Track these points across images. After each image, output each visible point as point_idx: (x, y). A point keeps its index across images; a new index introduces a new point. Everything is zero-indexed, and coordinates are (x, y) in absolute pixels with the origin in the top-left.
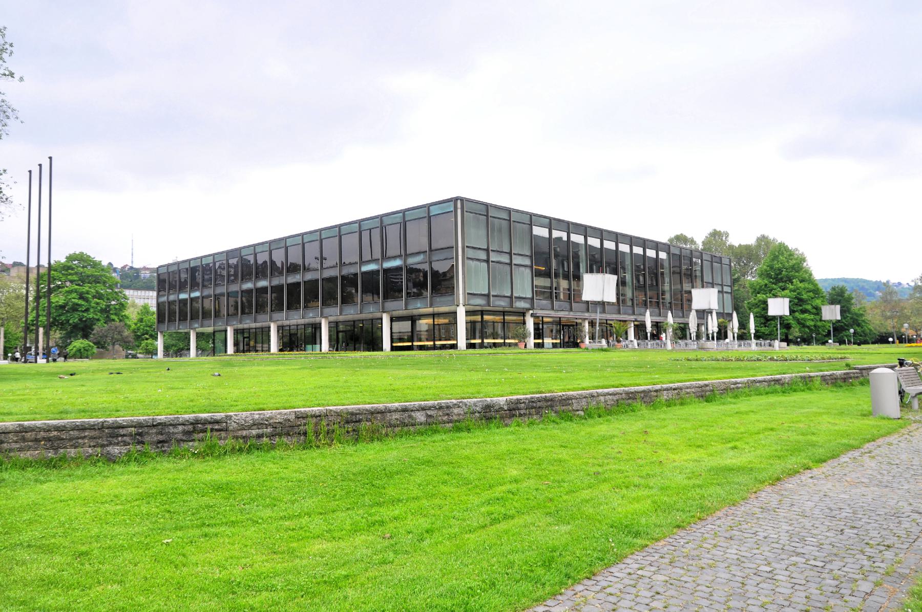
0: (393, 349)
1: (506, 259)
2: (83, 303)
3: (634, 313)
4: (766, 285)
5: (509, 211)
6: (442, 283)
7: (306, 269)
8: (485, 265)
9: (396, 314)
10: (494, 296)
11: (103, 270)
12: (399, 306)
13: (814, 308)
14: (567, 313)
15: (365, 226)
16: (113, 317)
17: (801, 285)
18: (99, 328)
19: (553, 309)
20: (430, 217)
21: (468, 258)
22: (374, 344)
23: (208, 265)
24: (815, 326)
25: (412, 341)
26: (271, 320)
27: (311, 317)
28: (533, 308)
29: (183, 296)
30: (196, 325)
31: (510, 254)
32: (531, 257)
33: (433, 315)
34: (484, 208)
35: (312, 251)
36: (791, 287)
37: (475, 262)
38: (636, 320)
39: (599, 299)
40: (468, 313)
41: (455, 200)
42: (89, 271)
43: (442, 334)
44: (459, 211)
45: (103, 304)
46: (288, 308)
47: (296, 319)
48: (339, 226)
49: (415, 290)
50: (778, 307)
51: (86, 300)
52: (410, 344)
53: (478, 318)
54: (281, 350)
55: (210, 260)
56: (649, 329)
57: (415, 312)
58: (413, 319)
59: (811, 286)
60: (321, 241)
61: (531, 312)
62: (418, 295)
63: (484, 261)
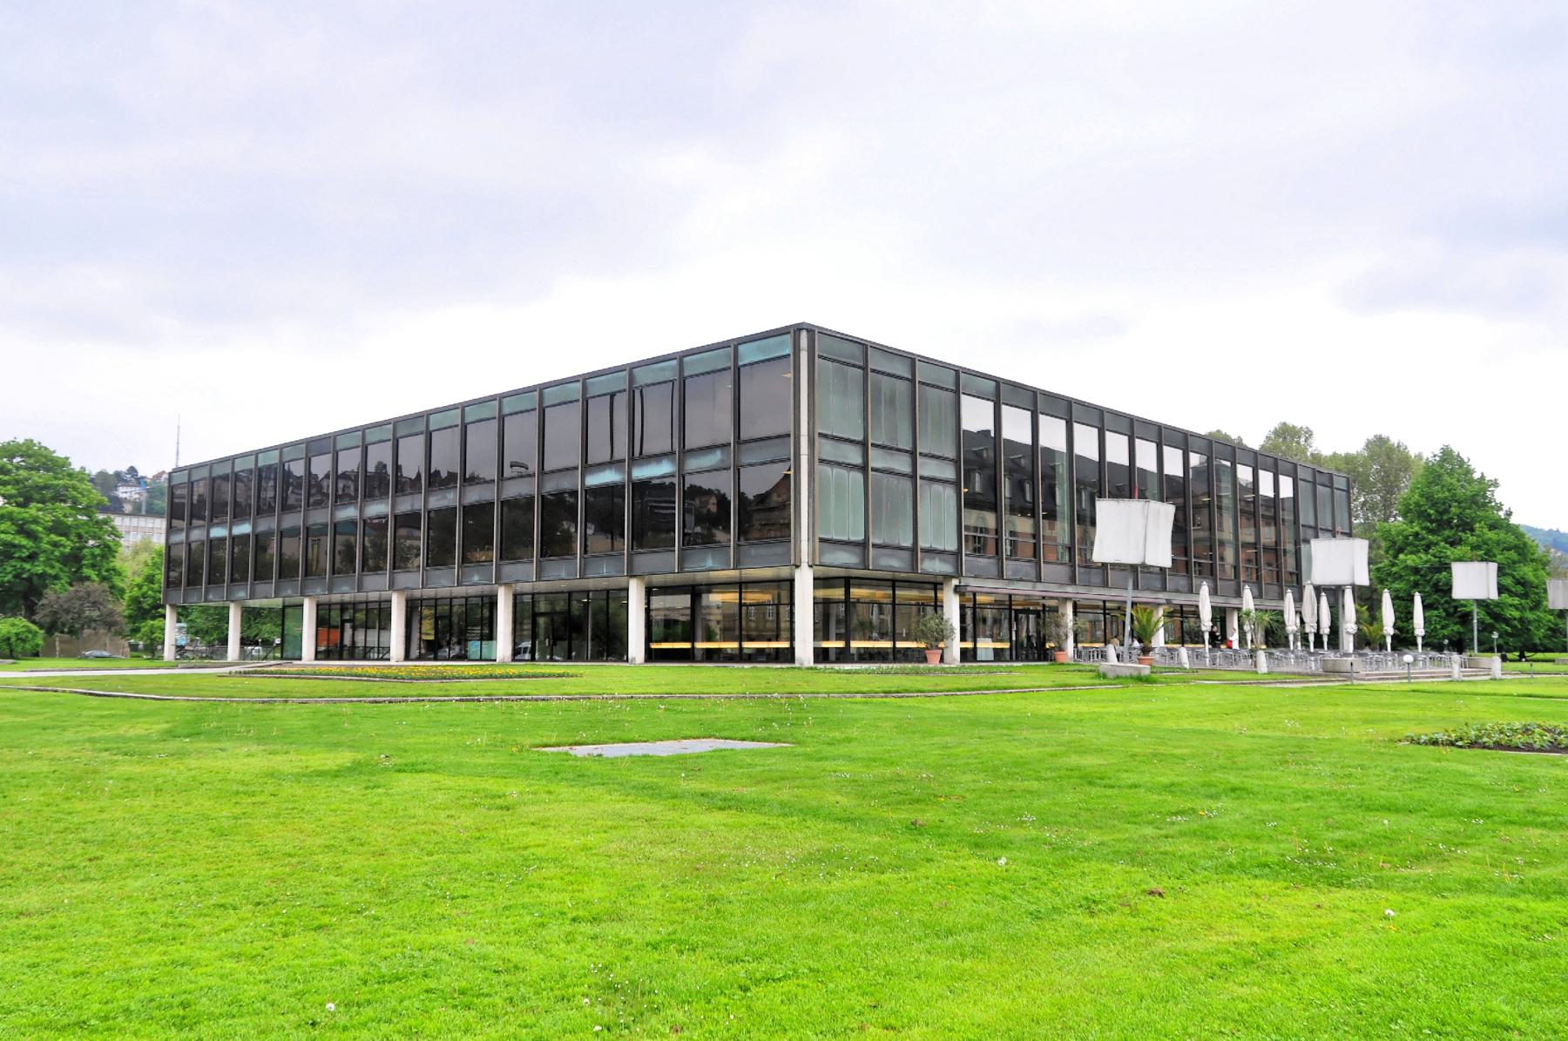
0: (652, 656)
1: (902, 464)
2: (24, 542)
3: (1164, 589)
4: (1416, 535)
5: (911, 360)
6: (766, 517)
7: (472, 480)
8: (859, 476)
9: (658, 580)
10: (874, 546)
11: (70, 475)
12: (664, 564)
13: (1518, 582)
14: (1029, 586)
15: (596, 387)
16: (87, 571)
17: (1491, 535)
18: (58, 593)
19: (1001, 576)
20: (738, 370)
21: (822, 461)
22: (611, 646)
23: (269, 467)
24: (1521, 620)
25: (692, 640)
26: (392, 587)
27: (475, 585)
28: (959, 575)
29: (218, 532)
30: (242, 594)
31: (913, 454)
32: (956, 462)
33: (741, 585)
34: (857, 350)
35: (482, 443)
36: (1472, 539)
37: (837, 470)
38: (1169, 602)
39: (1133, 559)
40: (820, 582)
41: (797, 330)
42: (40, 478)
43: (757, 633)
44: (804, 356)
45: (68, 545)
46: (543, 554)
47: (447, 585)
48: (541, 389)
49: (698, 529)
50: (1473, 582)
51: (31, 535)
52: (687, 645)
53: (838, 593)
54: (432, 649)
55: (273, 459)
56: (1206, 623)
57: (701, 577)
58: (696, 591)
59: (1511, 539)
60: (502, 419)
61: (955, 582)
62: (707, 541)
63: (854, 467)
